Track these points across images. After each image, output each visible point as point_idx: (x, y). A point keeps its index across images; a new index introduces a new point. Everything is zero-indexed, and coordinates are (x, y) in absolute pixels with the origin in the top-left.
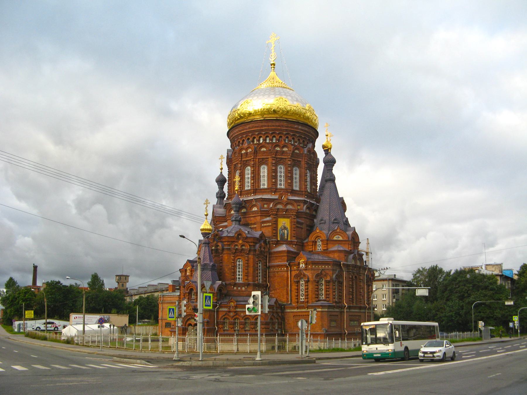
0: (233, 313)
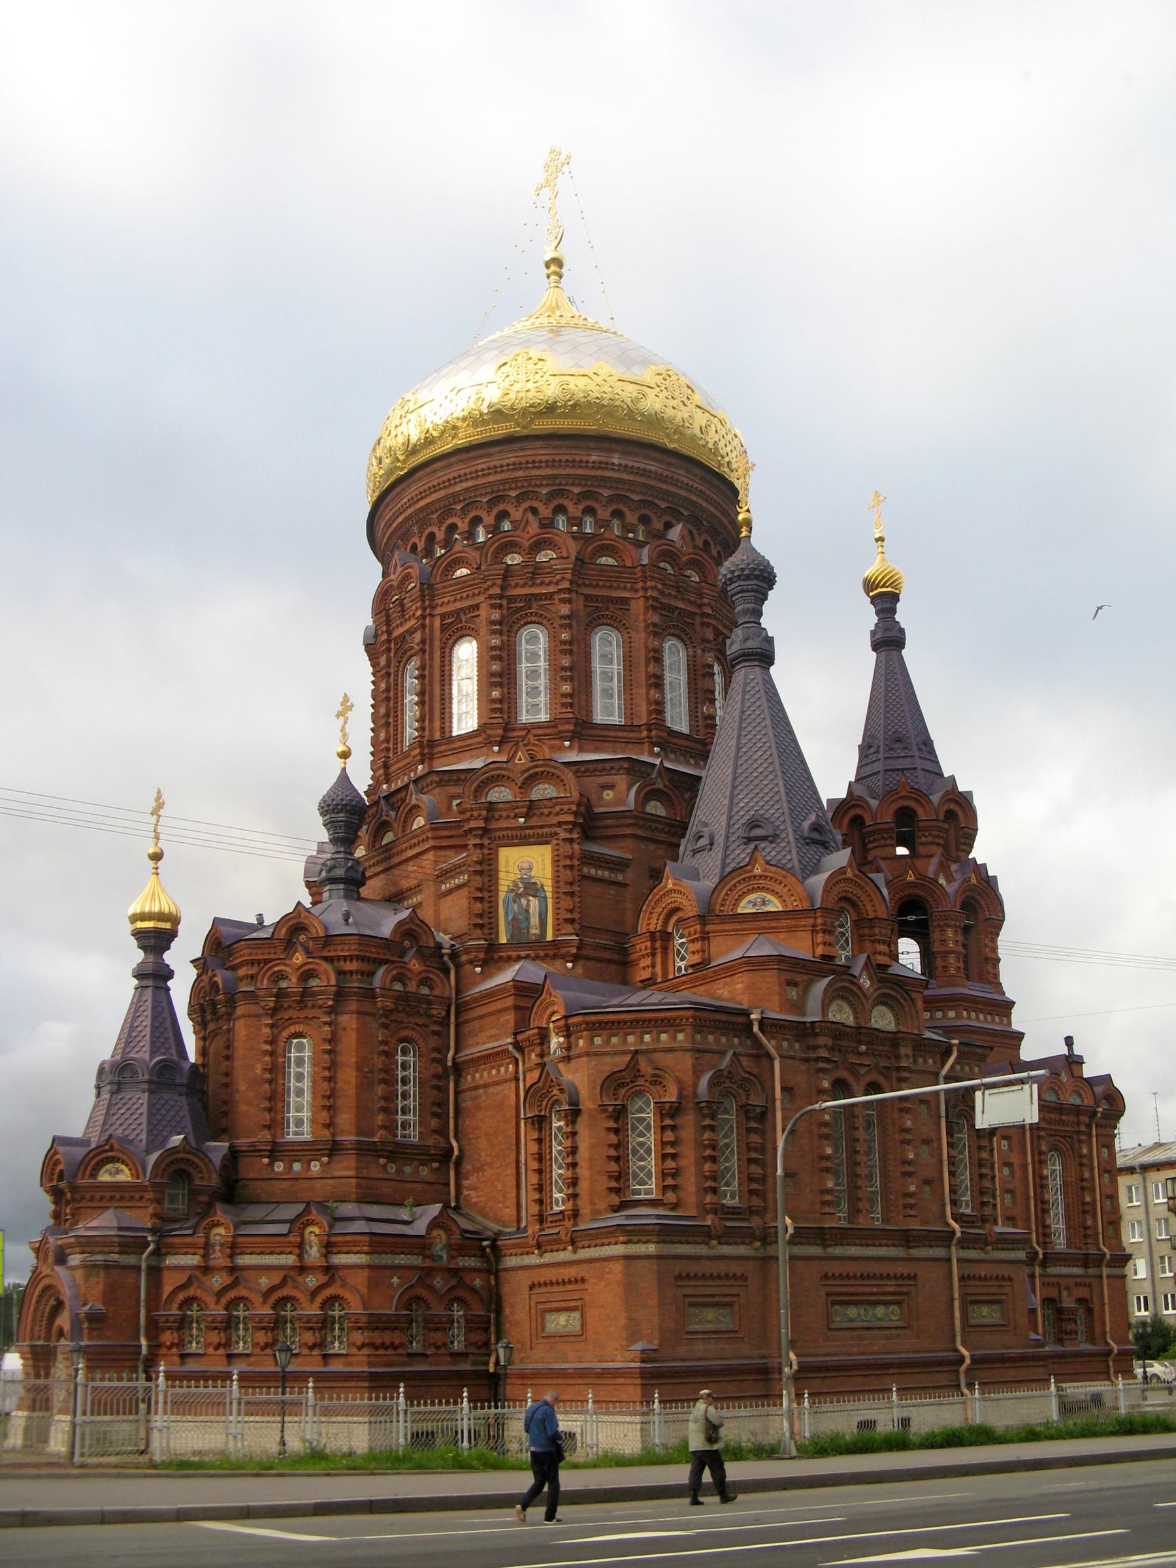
0: (224, 1274)
